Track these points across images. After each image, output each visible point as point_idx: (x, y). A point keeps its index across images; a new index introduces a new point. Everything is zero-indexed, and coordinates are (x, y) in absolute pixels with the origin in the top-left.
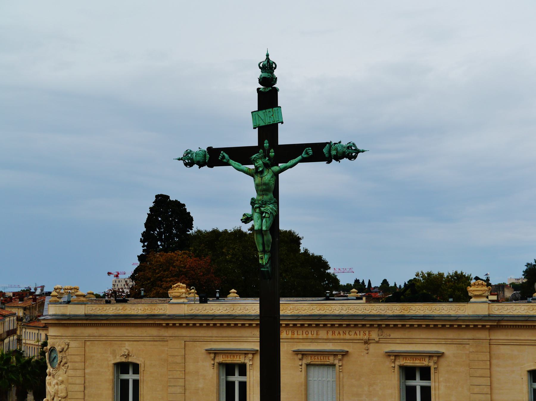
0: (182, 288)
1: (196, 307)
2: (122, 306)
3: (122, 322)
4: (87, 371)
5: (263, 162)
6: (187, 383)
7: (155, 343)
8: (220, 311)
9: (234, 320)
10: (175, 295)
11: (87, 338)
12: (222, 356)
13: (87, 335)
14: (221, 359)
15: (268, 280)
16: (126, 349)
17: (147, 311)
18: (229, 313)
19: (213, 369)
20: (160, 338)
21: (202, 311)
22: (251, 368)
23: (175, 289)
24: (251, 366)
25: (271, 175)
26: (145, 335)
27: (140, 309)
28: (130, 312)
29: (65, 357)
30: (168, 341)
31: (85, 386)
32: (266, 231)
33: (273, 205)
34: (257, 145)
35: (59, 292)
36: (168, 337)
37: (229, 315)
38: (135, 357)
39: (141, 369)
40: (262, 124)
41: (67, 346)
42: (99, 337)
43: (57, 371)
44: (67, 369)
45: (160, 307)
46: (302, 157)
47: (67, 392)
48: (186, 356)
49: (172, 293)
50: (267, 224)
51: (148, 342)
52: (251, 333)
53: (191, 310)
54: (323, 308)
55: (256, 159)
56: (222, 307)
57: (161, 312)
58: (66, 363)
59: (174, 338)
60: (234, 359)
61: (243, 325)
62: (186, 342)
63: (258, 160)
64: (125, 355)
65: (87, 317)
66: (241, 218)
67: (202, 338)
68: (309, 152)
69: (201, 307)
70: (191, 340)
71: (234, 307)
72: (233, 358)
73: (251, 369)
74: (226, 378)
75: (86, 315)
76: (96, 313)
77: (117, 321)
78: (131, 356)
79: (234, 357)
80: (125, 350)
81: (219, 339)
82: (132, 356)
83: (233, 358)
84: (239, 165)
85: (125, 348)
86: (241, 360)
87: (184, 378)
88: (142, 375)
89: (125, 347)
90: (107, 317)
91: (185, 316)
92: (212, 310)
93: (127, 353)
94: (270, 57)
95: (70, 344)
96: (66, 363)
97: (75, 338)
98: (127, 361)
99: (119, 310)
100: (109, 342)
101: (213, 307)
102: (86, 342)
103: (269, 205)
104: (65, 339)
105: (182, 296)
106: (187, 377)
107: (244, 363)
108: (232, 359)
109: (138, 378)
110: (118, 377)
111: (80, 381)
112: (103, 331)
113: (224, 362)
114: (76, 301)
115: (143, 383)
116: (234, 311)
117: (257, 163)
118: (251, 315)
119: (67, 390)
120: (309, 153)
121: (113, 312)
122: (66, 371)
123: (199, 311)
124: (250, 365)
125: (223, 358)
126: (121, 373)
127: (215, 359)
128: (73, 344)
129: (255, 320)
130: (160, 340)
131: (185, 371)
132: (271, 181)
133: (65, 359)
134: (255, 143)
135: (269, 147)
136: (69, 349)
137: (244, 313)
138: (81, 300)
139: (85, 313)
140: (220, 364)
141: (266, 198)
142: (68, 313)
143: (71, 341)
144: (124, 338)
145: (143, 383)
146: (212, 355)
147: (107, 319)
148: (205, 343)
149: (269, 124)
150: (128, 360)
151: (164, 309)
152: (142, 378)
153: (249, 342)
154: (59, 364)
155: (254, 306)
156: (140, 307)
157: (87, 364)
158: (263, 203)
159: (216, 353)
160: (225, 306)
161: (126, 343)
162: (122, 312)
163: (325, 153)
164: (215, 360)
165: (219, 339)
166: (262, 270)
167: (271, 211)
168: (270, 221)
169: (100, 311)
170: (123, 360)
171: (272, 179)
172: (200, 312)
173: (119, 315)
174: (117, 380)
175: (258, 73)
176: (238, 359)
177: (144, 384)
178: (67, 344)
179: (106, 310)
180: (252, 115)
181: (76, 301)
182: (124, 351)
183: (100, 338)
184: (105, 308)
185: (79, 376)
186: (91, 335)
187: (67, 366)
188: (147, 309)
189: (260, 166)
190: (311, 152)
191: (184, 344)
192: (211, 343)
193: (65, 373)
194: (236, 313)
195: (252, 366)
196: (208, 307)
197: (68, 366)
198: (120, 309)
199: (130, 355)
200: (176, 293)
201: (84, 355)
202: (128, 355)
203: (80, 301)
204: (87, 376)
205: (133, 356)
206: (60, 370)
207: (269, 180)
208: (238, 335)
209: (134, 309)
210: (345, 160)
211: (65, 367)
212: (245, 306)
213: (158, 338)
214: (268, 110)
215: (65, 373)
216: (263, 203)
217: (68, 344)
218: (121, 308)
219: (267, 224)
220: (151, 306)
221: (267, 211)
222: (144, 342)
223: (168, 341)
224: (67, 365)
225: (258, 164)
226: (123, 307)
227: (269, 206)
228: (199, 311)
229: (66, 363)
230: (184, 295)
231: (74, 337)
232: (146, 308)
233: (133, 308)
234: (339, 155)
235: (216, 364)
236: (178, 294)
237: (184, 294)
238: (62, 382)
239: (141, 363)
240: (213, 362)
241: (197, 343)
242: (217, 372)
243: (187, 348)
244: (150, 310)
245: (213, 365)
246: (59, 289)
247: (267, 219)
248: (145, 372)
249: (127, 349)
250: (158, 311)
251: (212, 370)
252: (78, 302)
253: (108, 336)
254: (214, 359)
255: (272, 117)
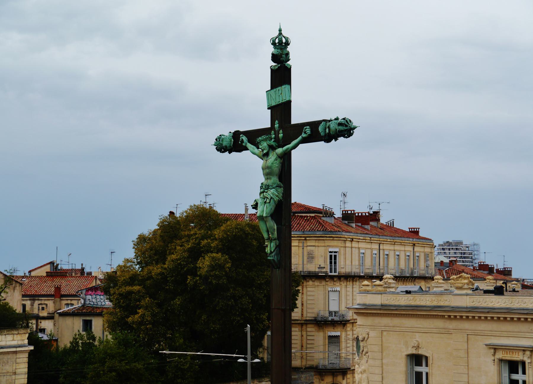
0: (465, 278)
1: (477, 299)
2: (412, 296)
3: (407, 313)
4: (384, 361)
5: (268, 145)
6: (470, 378)
7: (442, 335)
8: (499, 304)
9: (509, 314)
10: (457, 286)
11: (383, 328)
12: (501, 352)
13: (383, 325)
14: (500, 355)
15: (278, 269)
16: (415, 341)
17: (434, 302)
18: (508, 306)
19: (494, 365)
20: (445, 330)
21: (522, 304)
22: (530, 366)
23: (459, 280)
24: (529, 364)
25: (275, 157)
26: (432, 326)
27: (428, 300)
28: (420, 302)
29: (366, 346)
30: (452, 334)
31: (383, 377)
32: (266, 217)
33: (275, 190)
34: (269, 126)
35: (387, 282)
36: (452, 330)
37: (507, 309)
38: (424, 349)
39: (430, 362)
40: (274, 104)
41: (367, 335)
42: (393, 328)
43: (360, 360)
44: (368, 358)
45: (446, 299)
46: (302, 137)
47: (369, 382)
48: (469, 350)
49: (455, 284)
50: (267, 210)
51: (436, 334)
52: (529, 328)
53: (473, 302)
54: (398, 298)
55: (260, 142)
56: (501, 299)
57: (446, 304)
58: (367, 353)
59: (460, 331)
60: (513, 356)
61: (519, 319)
62: (469, 336)
63: (262, 142)
64: (415, 347)
65: (383, 307)
66: (252, 204)
67: (483, 332)
68: (307, 131)
69: (482, 299)
70: (473, 334)
71: (513, 299)
72: (512, 355)
73: (530, 368)
74: (509, 376)
75: (382, 305)
76: (391, 303)
77: (406, 312)
78: (421, 348)
79: (513, 353)
80: (415, 342)
81: (498, 333)
82: (422, 348)
83: (512, 355)
84: (253, 149)
85: (415, 340)
86: (519, 357)
87: (467, 373)
88: (431, 368)
89: (415, 338)
90: (398, 308)
91: (467, 308)
92: (524, 303)
93: (416, 345)
94: (282, 32)
95: (370, 334)
96: (367, 353)
97: (373, 327)
98: (417, 353)
99: (410, 301)
100: (402, 333)
101: (526, 300)
102: (383, 332)
103: (271, 189)
104: (366, 329)
105: (464, 287)
106: (470, 372)
107: (523, 360)
108: (511, 356)
109: (427, 371)
110: (413, 369)
111: (378, 371)
112: (396, 321)
113: (503, 358)
114: (374, 291)
115: (432, 377)
116: (512, 304)
117: (261, 145)
118: (528, 309)
119: (368, 380)
120: (307, 132)
121: (405, 302)
122: (367, 360)
123: (480, 303)
124: (528, 363)
125: (503, 354)
126: (416, 365)
127: (496, 355)
128: (372, 334)
129: (529, 314)
130: (446, 332)
131: (468, 366)
132: (274, 164)
133: (366, 348)
134: (268, 125)
135: (279, 128)
136: (369, 338)
137: (522, 306)
138: (378, 290)
139: (381, 303)
140: (501, 360)
141: (270, 182)
142: (368, 302)
143: (370, 331)
144: (415, 329)
145: (432, 377)
146: (492, 351)
147: (469, 311)
148: (486, 337)
149: (278, 103)
150: (418, 352)
151: (448, 300)
152: (431, 371)
153: (528, 338)
154: (362, 354)
155: (531, 299)
156: (428, 298)
157: (384, 354)
158: (266, 188)
159: (495, 348)
160: (504, 298)
161: (417, 334)
162: (413, 303)
163: (320, 132)
164: (495, 356)
165: (498, 333)
166: (269, 259)
167: (271, 195)
168: (270, 207)
169: (394, 301)
170: (414, 352)
171: (275, 162)
172: (506, 304)
173: (410, 306)
174: (410, 373)
175: (271, 49)
176: (517, 356)
177: (433, 377)
178: (367, 333)
179: (400, 301)
180: (268, 95)
181: (374, 291)
182: (414, 343)
183: (395, 328)
184: (398, 298)
185: (377, 366)
186: (386, 326)
187: (368, 356)
188: (434, 300)
189: (265, 148)
190: (308, 131)
191: (466, 337)
192: (492, 337)
193: (367, 362)
194: (515, 306)
195: (531, 364)
196: (488, 299)
197: (369, 355)
198: (411, 299)
199: (420, 347)
200: (459, 284)
201: (382, 345)
202: (418, 347)
203: (377, 291)
204: (384, 367)
205: (423, 348)
206: (363, 359)
207: (272, 163)
208: (516, 330)
209: (423, 300)
210: (341, 139)
211: (366, 357)
212: (523, 299)
213: (444, 330)
214: (277, 89)
215: (367, 362)
216: (266, 188)
217: (368, 333)
218: (412, 298)
219: (267, 210)
220: (437, 297)
221: (268, 196)
222: (432, 334)
223: (452, 334)
224: (367, 354)
225: (262, 146)
226: (413, 297)
227: (270, 191)
228: (480, 303)
229: (367, 352)
230: (466, 286)
231: (373, 327)
232: (434, 298)
233: (422, 298)
234: (332, 133)
235: (496, 360)
236: (460, 285)
237: (466, 285)
238: (365, 371)
239: (430, 356)
240: (493, 358)
241: (479, 336)
242: (498, 368)
243: (469, 342)
244: (437, 302)
245: (493, 361)
246: (388, 278)
247: (268, 204)
248: (433, 365)
249: (417, 341)
250: (444, 302)
251: (493, 366)
252: (377, 292)
253: (400, 326)
254: (494, 355)
255: (281, 95)
